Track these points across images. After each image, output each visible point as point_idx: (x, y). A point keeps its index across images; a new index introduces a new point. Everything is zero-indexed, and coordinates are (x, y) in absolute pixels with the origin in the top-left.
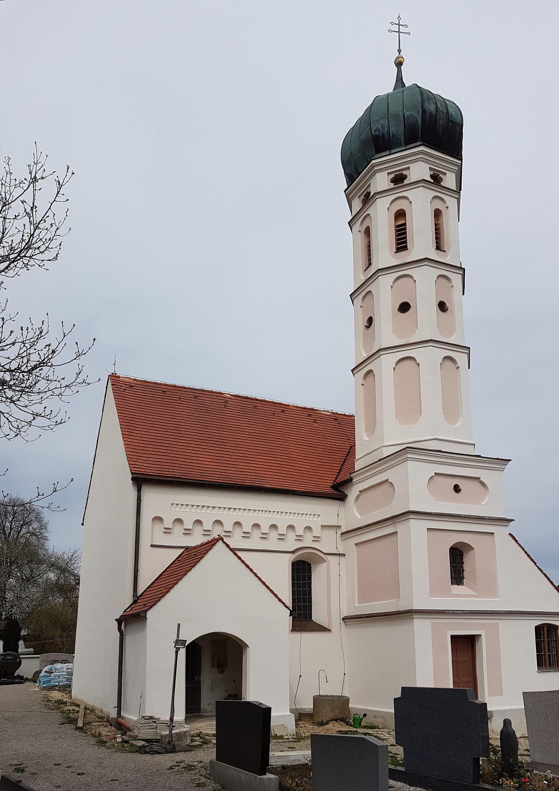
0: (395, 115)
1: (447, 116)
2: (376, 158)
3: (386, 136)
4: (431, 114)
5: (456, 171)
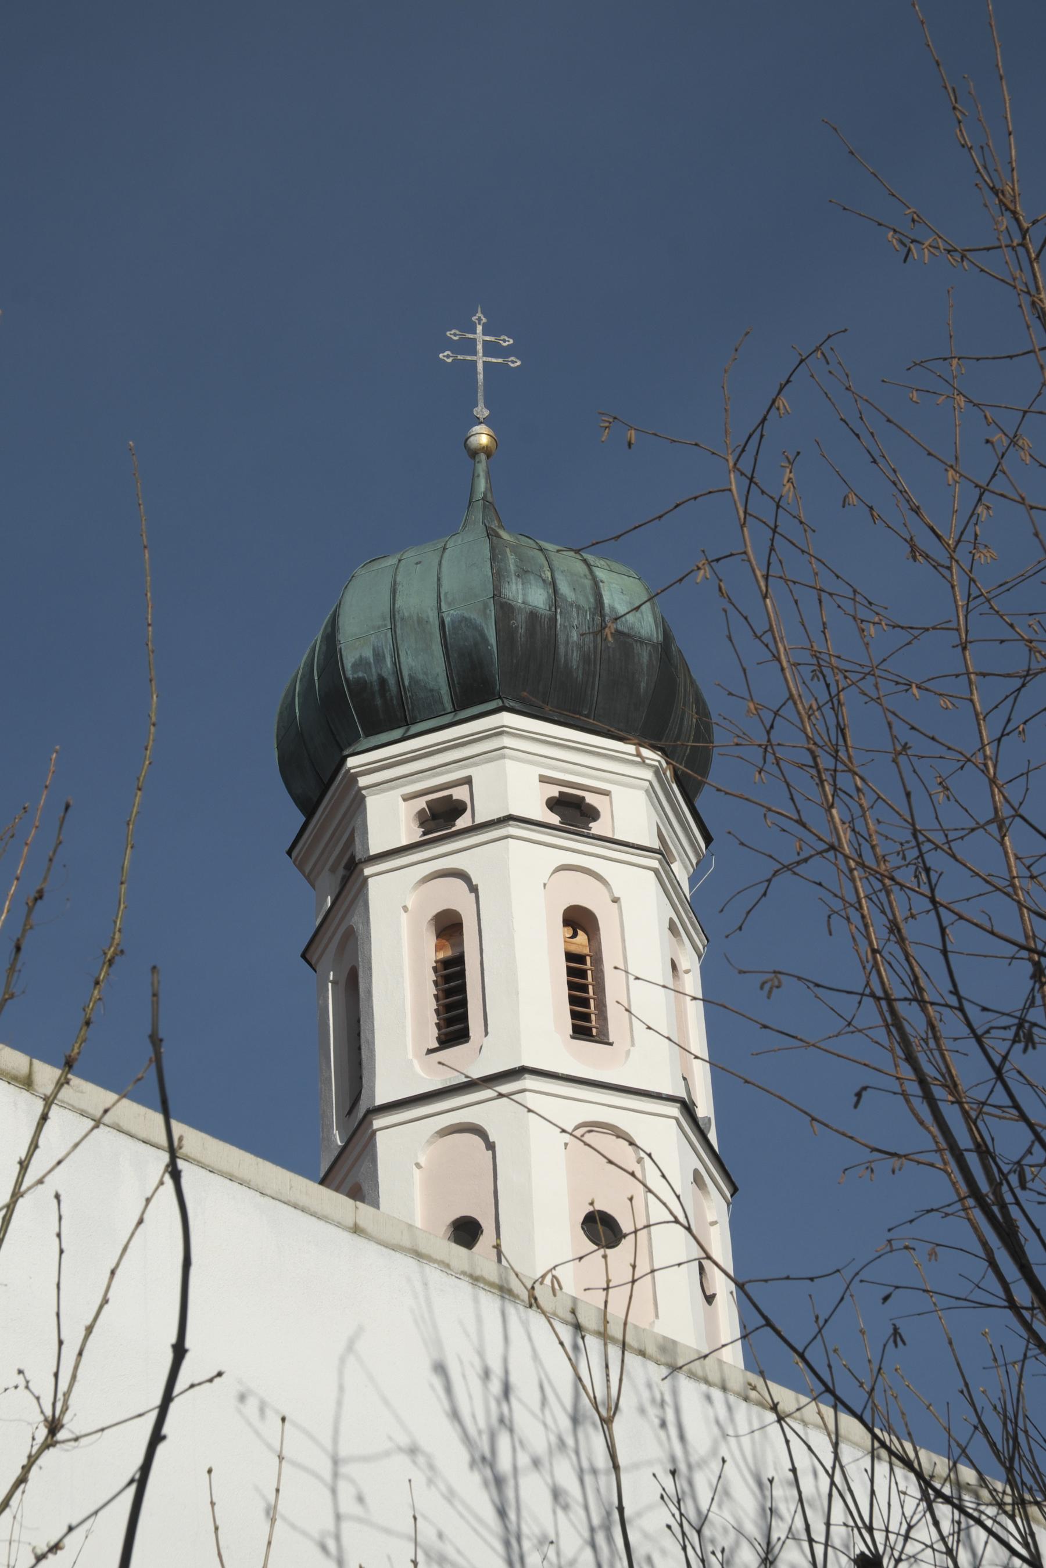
0: (415, 618)
1: (598, 618)
2: (359, 749)
3: (392, 681)
4: (533, 616)
5: (647, 784)
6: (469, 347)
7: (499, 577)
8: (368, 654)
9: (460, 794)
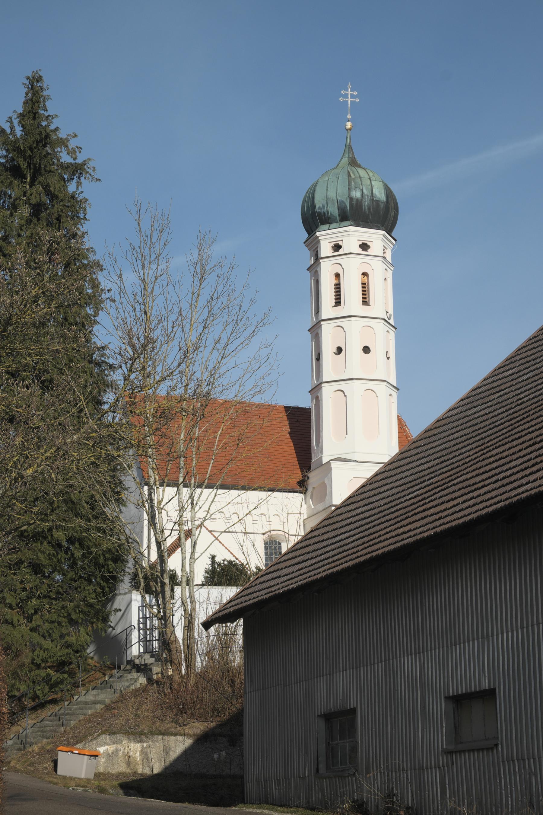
3: (326, 213)
4: (357, 200)
6: (346, 96)
7: (350, 190)
8: (321, 206)
9: (340, 243)
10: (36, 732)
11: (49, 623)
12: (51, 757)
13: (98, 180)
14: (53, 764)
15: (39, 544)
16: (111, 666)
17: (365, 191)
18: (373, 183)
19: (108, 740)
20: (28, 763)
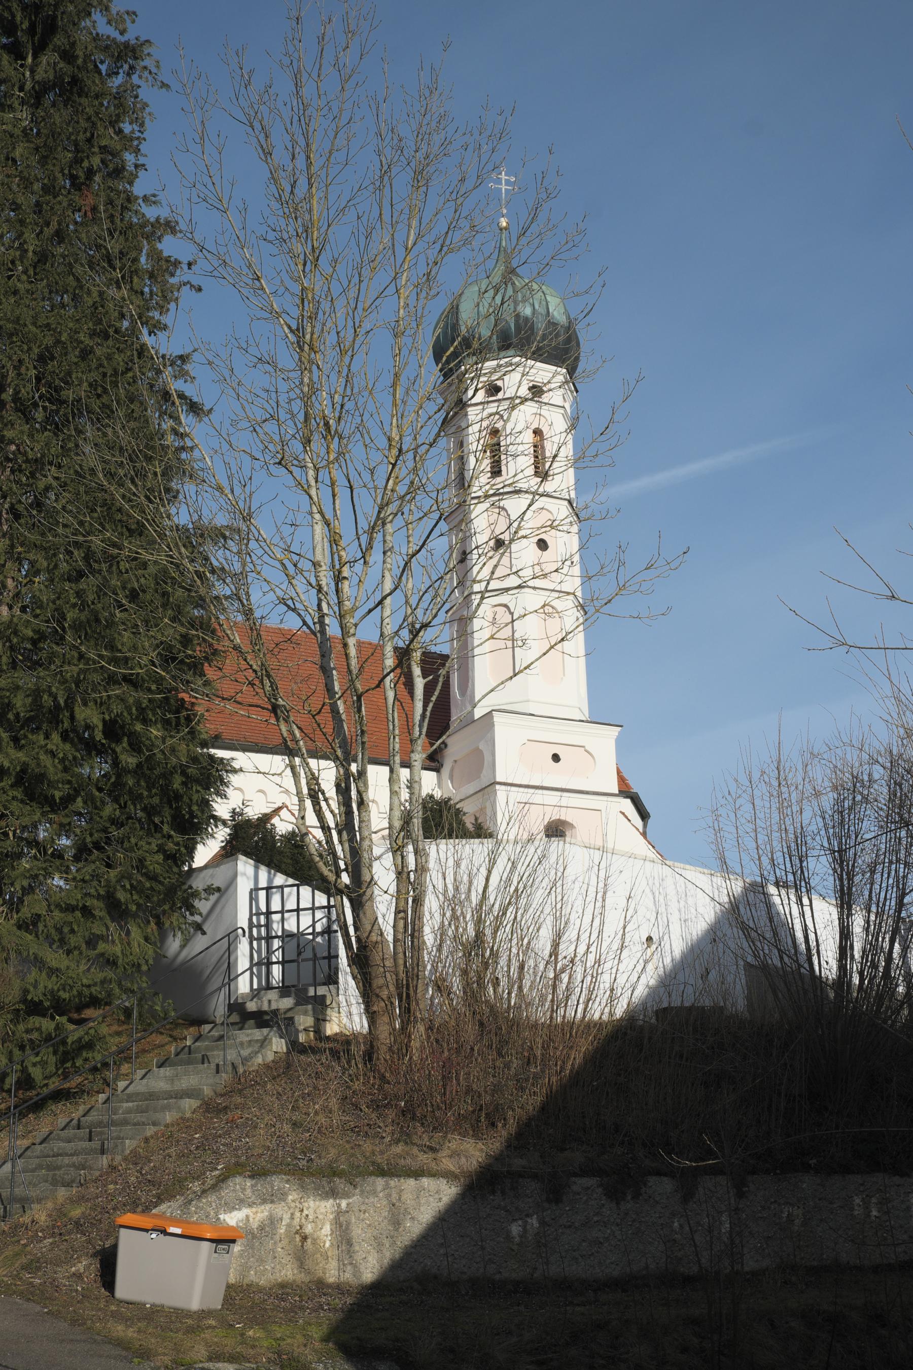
6: (499, 181)
10: (33, 1171)
11: (62, 910)
12: (89, 1242)
13: (164, 85)
14: (96, 1265)
15: (42, 737)
16: (181, 1021)
17: (537, 307)
18: (549, 298)
19: (249, 1192)
20: (24, 1260)
